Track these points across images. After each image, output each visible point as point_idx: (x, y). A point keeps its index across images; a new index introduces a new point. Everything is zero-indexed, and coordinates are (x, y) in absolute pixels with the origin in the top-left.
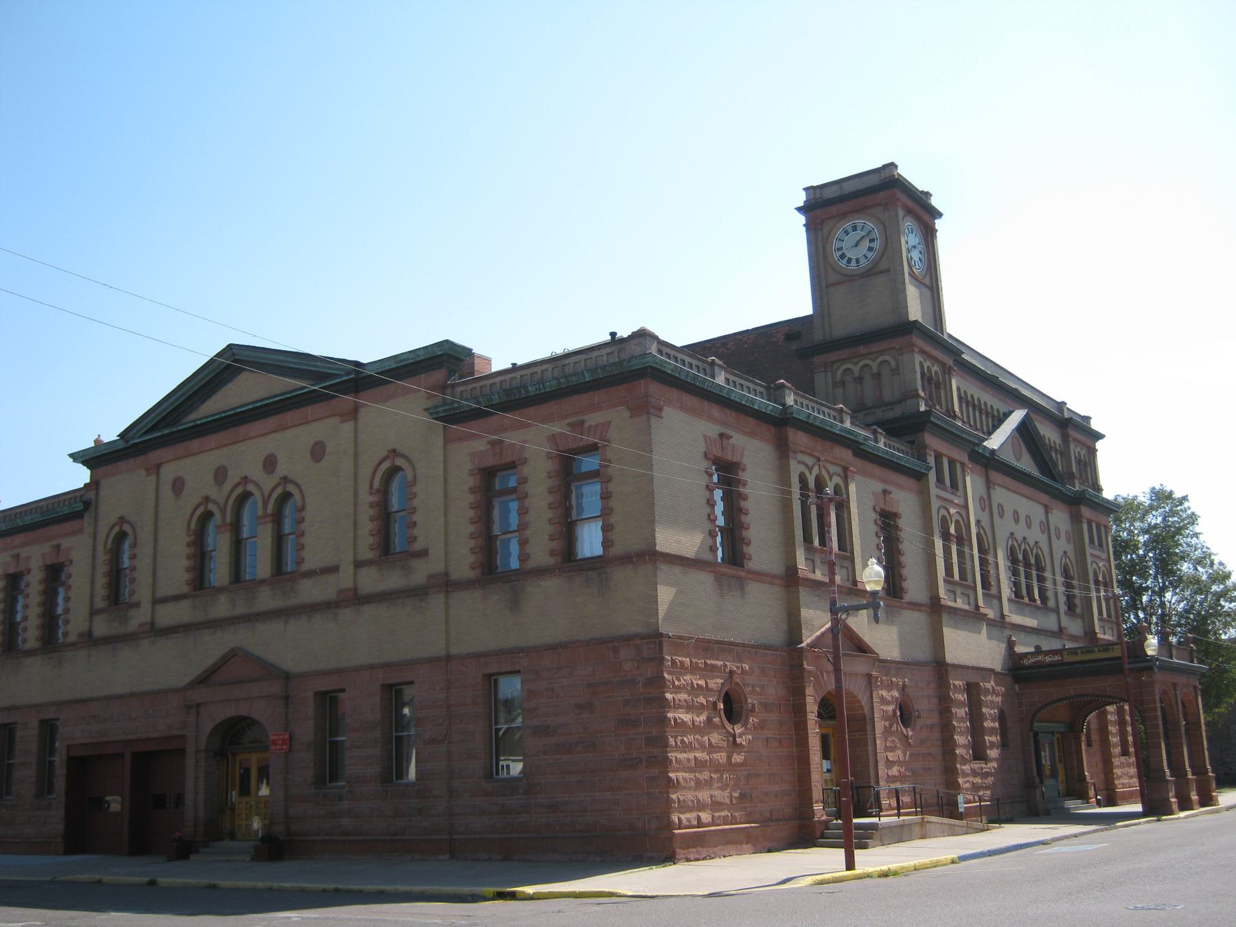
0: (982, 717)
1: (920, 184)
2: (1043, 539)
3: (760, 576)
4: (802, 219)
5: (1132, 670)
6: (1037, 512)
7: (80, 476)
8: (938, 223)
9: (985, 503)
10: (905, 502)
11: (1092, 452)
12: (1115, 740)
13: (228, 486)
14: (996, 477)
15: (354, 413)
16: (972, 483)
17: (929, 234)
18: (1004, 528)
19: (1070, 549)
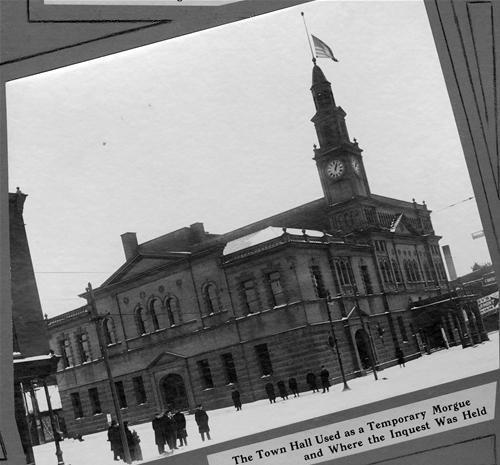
0: (404, 328)
1: (328, 79)
2: (415, 258)
3: (376, 296)
4: (315, 162)
5: (352, 282)
6: (412, 248)
7: (84, 302)
8: (362, 154)
9: (395, 252)
10: (368, 262)
11: (429, 218)
12: (452, 324)
13: (147, 299)
14: (397, 240)
15: (190, 268)
16: (390, 246)
17: (359, 159)
18: (402, 258)
19: (426, 259)
